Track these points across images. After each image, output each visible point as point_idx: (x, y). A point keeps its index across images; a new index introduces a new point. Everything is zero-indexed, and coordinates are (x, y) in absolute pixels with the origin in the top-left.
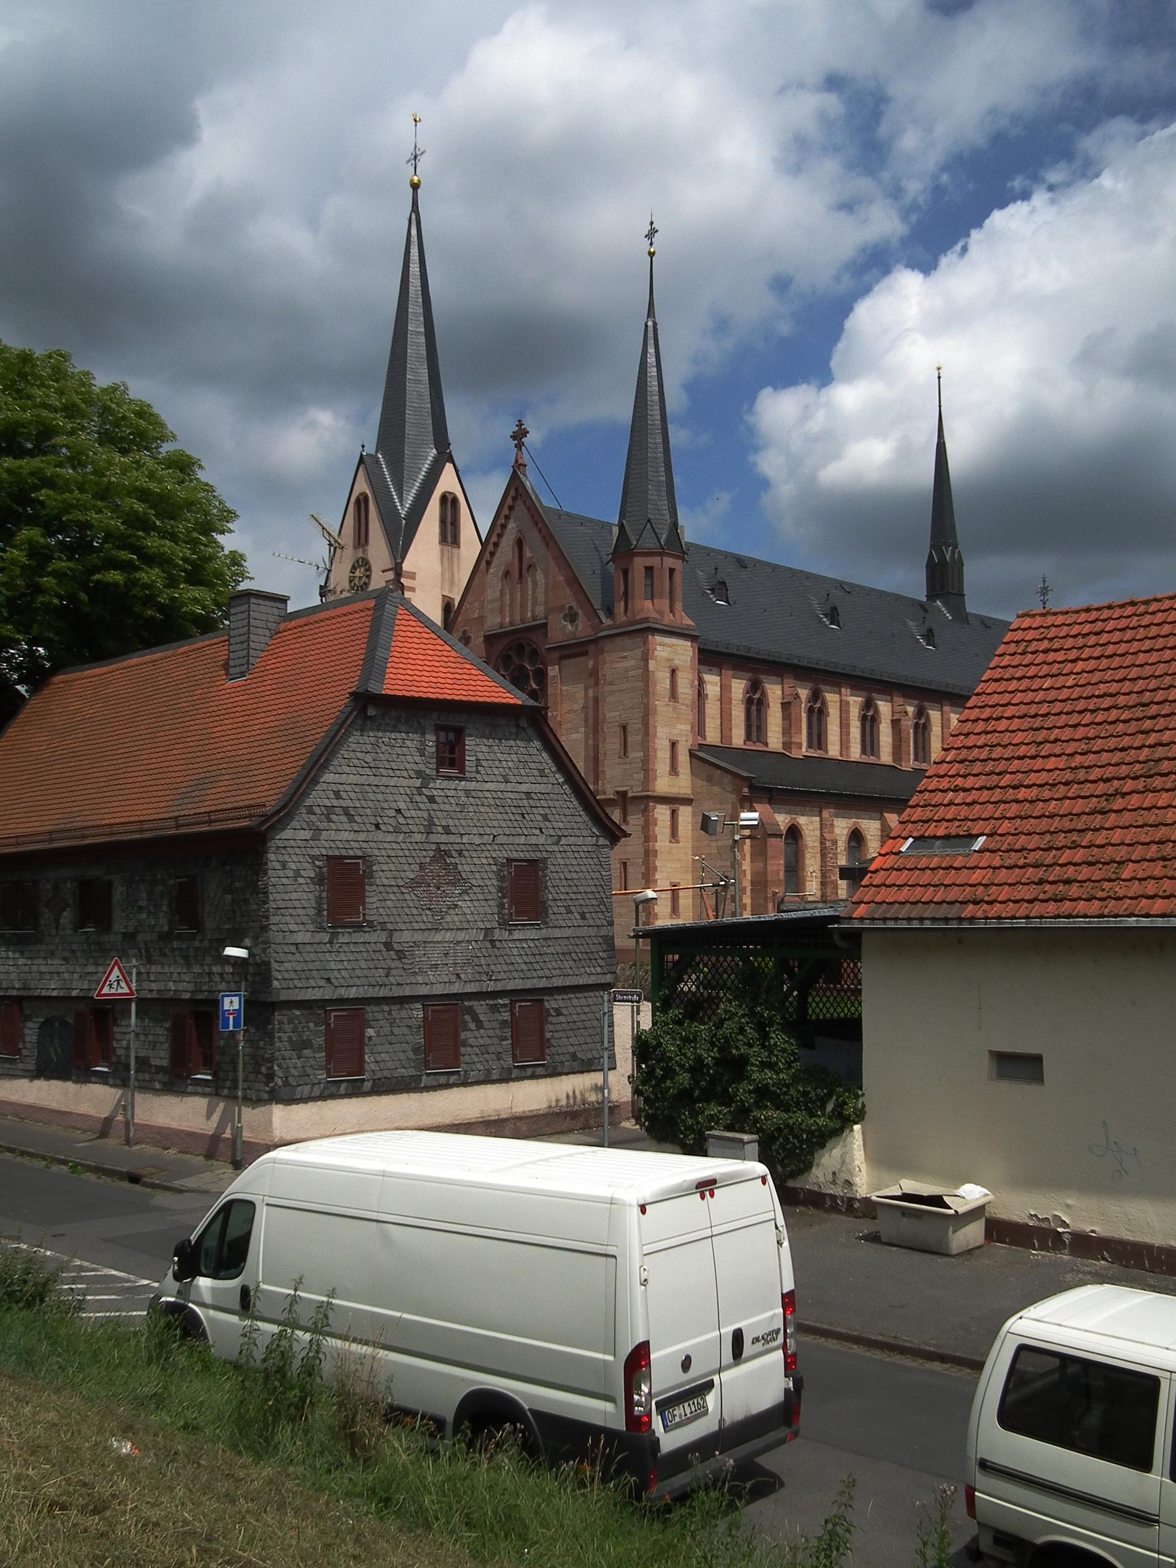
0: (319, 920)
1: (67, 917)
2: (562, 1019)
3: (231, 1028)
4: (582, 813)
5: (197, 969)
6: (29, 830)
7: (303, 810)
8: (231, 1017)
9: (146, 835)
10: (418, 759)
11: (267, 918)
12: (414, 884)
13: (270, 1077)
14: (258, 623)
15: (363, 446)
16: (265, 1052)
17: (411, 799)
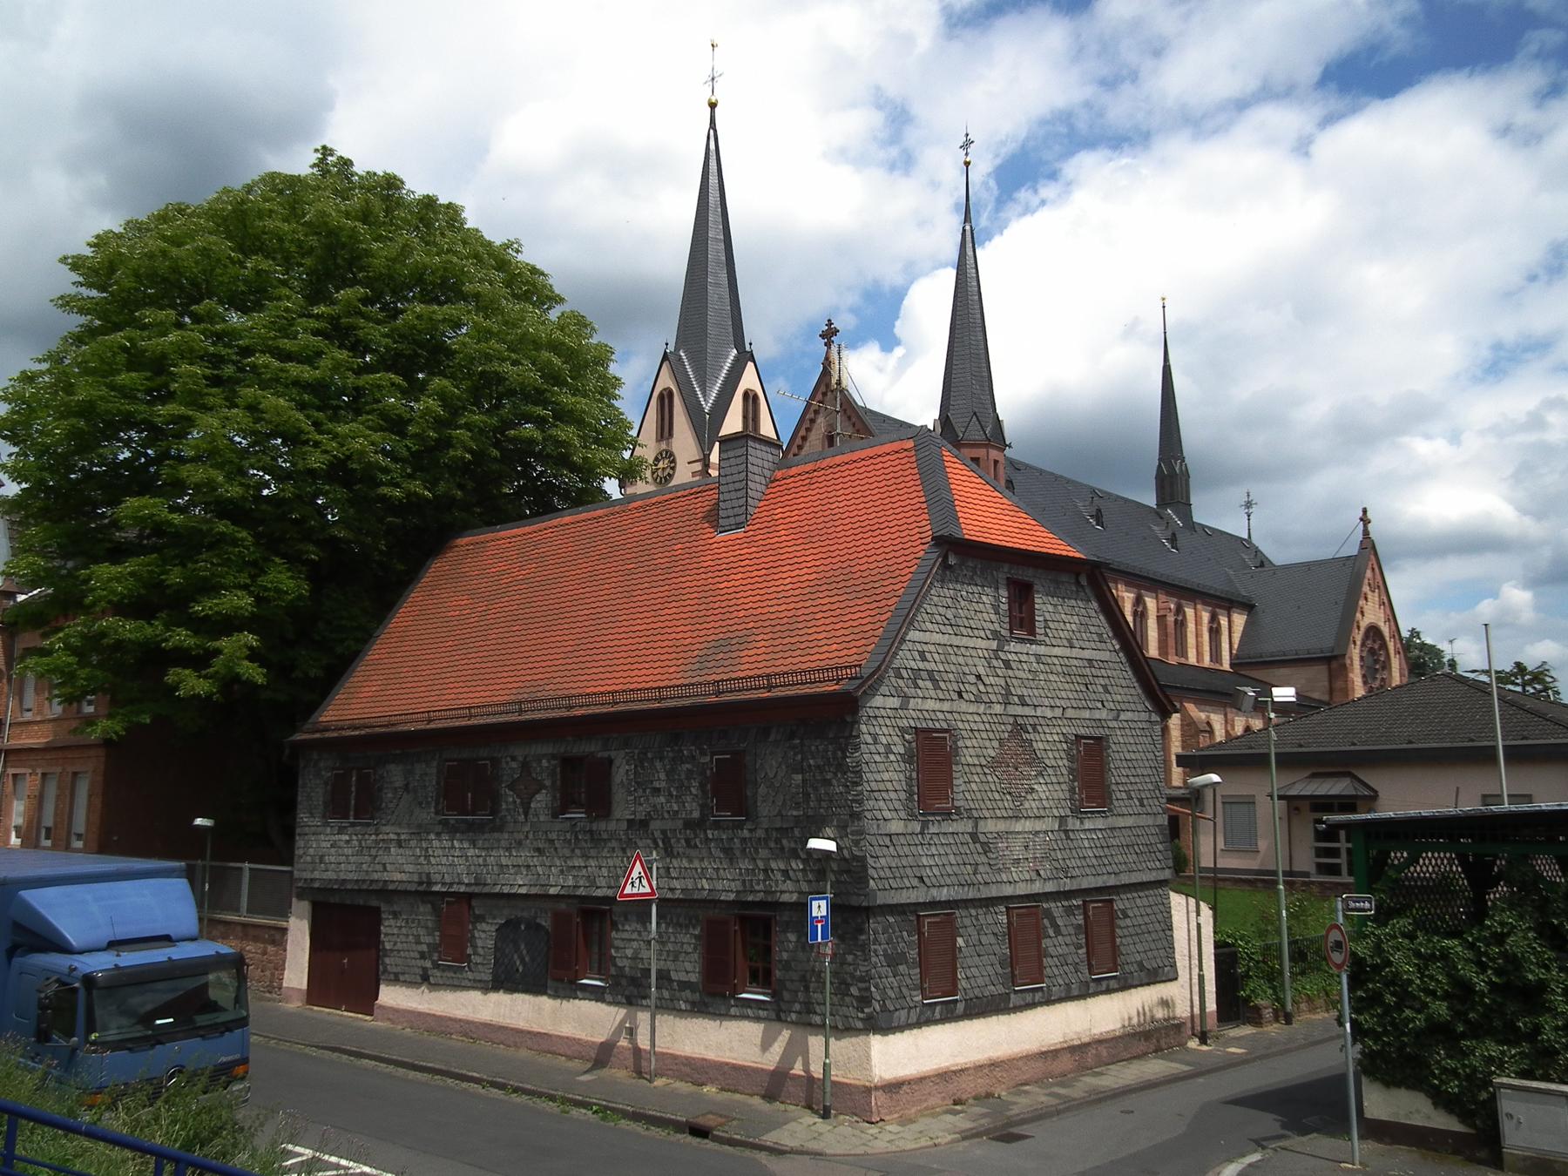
0: (910, 805)
1: (541, 801)
2: (1128, 921)
3: (819, 940)
4: (1136, 685)
5: (745, 864)
6: (476, 701)
7: (891, 673)
8: (819, 925)
9: (777, 693)
10: (994, 617)
11: (860, 802)
12: (995, 763)
13: (865, 1000)
14: (756, 470)
15: (667, 344)
16: (855, 970)
17: (989, 664)
